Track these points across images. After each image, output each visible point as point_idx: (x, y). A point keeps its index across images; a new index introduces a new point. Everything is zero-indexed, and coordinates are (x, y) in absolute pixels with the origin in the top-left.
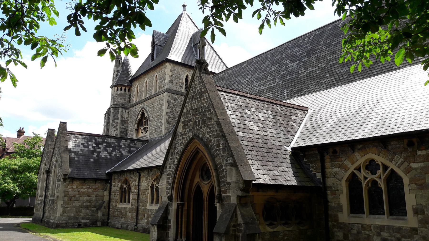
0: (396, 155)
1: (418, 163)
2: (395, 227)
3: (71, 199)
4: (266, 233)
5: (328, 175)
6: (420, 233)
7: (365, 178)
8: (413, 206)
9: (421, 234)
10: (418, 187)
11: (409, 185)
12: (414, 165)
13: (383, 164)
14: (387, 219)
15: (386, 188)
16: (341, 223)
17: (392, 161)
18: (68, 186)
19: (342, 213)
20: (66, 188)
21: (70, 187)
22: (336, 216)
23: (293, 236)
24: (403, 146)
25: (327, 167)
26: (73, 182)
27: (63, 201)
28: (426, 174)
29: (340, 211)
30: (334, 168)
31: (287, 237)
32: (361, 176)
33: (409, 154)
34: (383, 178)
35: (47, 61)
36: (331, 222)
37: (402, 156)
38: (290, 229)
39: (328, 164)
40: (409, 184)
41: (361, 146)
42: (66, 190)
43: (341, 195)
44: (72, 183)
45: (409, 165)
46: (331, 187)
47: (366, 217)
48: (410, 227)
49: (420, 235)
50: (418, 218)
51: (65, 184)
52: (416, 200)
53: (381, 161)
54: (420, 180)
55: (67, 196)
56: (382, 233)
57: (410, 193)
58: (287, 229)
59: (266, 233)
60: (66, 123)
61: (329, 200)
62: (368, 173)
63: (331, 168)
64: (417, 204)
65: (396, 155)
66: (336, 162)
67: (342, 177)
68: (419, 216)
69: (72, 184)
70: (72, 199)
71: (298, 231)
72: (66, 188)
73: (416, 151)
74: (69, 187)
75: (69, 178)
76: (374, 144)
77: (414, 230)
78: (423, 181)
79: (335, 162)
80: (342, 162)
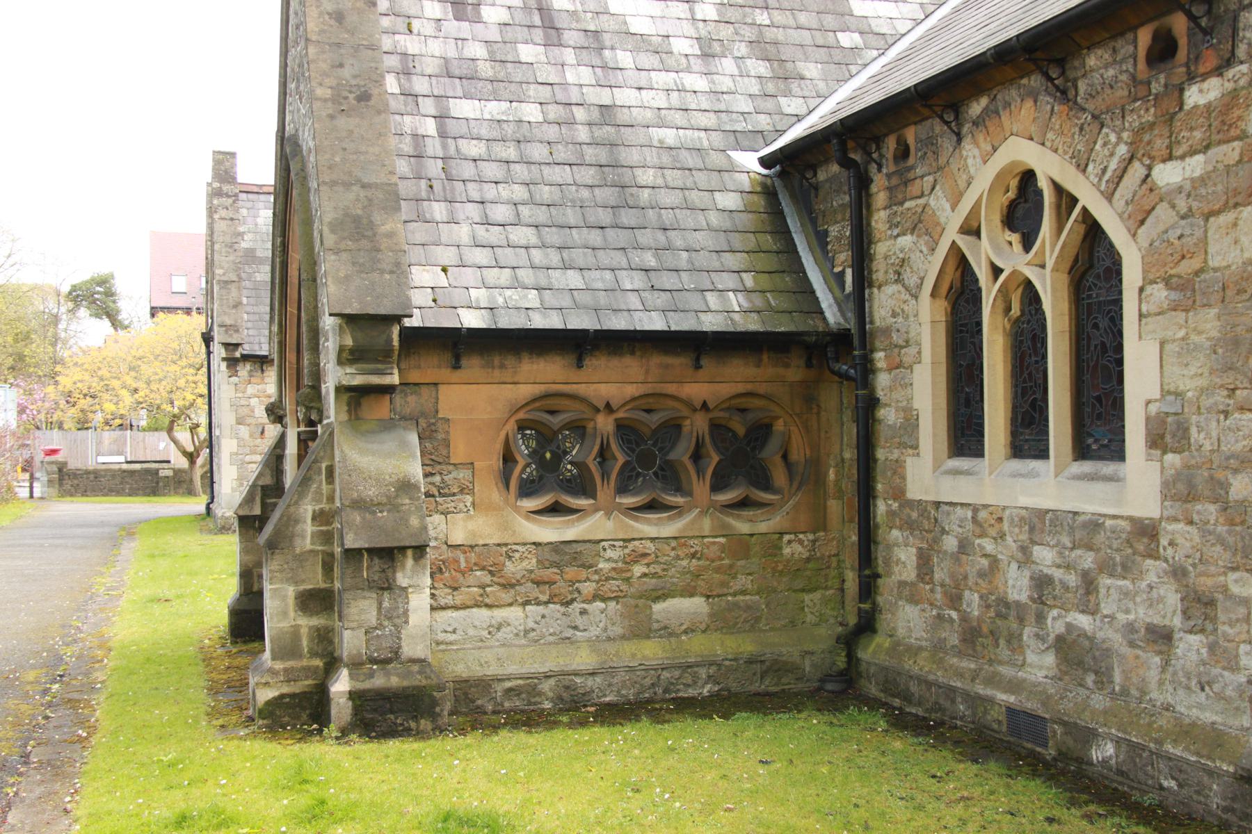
0: (1105, 130)
1: (1182, 157)
2: (1081, 518)
3: (262, 432)
4: (515, 547)
5: (880, 270)
6: (1165, 549)
7: (996, 271)
8: (1148, 402)
9: (1170, 551)
10: (1174, 295)
11: (1141, 290)
12: (1168, 175)
13: (1058, 189)
14: (1056, 476)
15: (1067, 318)
16: (911, 504)
17: (1087, 165)
18: (246, 388)
19: (918, 455)
20: (240, 395)
21: (255, 392)
22: (898, 466)
23: (685, 563)
24: (1131, 70)
25: (878, 236)
26: (263, 371)
27: (235, 442)
28: (1212, 219)
29: (911, 447)
30: (898, 235)
31: (648, 565)
32: (981, 255)
33: (1152, 110)
34: (1050, 264)
35: (1013, 162)
36: (885, 499)
37: (1124, 129)
38: (670, 528)
39: (879, 220)
40: (1140, 284)
41: (984, 101)
42: (243, 402)
43: (916, 367)
44: (259, 373)
45: (1148, 176)
46: (887, 331)
47: (1052, 473)
48: (1131, 519)
49: (1166, 561)
50: (1163, 468)
51: (235, 379)
52: (1161, 373)
53: (1058, 179)
54: (1183, 257)
55: (249, 420)
56: (1036, 548)
57: (1140, 338)
58: (651, 531)
59: (515, 547)
60: (233, 155)
61: (880, 393)
62: (1010, 243)
63: (891, 236)
64: (1165, 393)
65: (1102, 126)
66: (908, 204)
67: (922, 275)
68: (1170, 458)
69: (263, 379)
70: (266, 432)
71: (722, 540)
72: (240, 395)
73: (1182, 91)
74: (251, 390)
75: (246, 358)
76: (1025, 81)
77: (1146, 531)
78: (1195, 264)
79: (901, 204)
80: (922, 201)
